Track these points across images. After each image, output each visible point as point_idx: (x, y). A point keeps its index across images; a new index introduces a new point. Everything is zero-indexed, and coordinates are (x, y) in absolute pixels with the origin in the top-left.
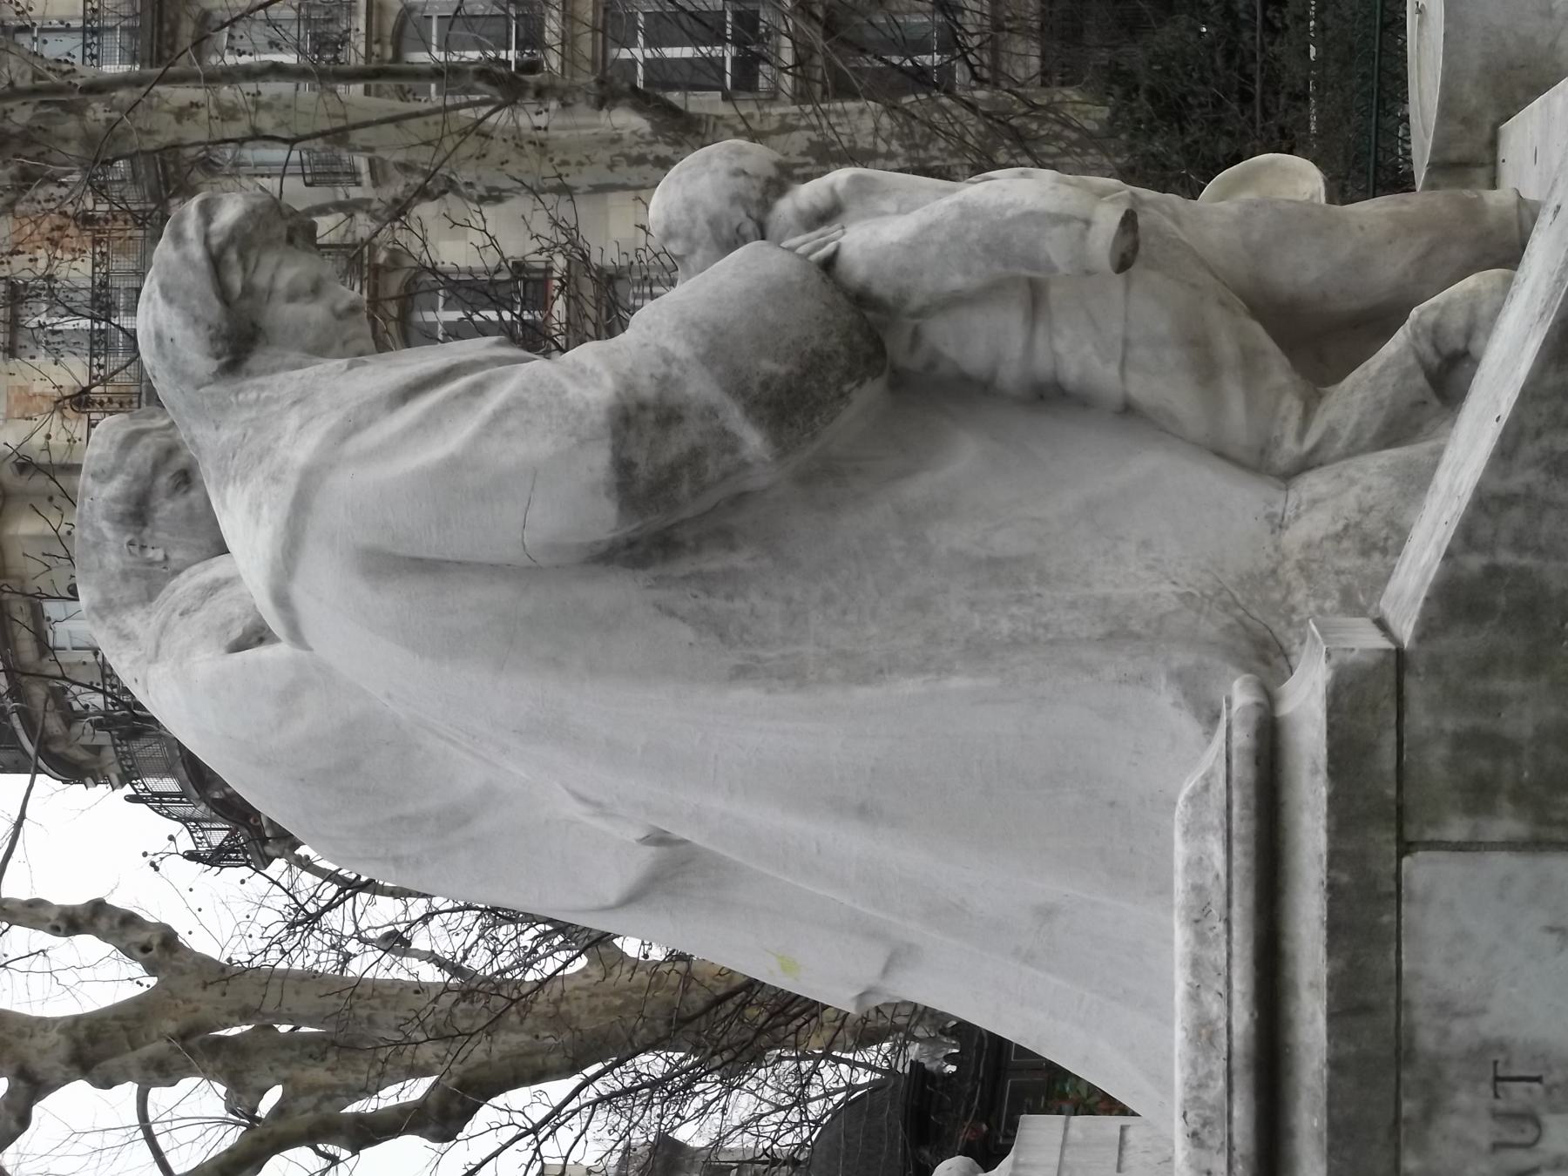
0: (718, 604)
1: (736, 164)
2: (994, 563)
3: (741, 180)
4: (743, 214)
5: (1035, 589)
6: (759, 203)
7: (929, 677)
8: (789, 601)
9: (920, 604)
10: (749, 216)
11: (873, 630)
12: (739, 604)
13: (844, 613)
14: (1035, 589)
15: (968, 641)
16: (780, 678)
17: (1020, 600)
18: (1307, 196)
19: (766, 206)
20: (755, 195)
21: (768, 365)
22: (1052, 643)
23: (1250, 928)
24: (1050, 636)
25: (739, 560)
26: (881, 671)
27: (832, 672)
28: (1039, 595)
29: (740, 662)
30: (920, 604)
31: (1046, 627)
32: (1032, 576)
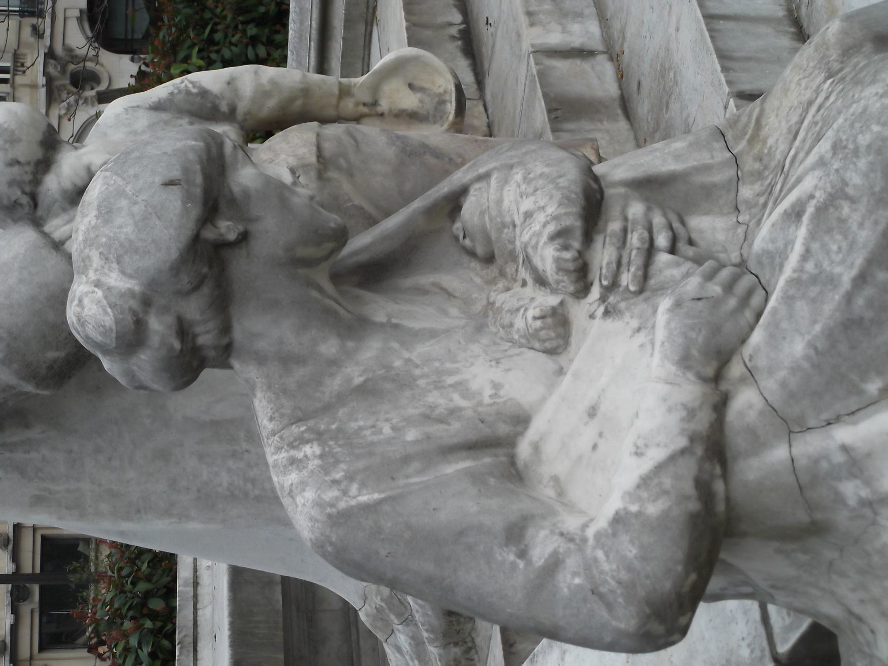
0: (19, 456)
1: (11, 155)
2: (215, 424)
3: (16, 169)
4: (19, 193)
5: (245, 446)
6: (30, 182)
7: (172, 520)
8: (70, 452)
9: (163, 455)
10: (24, 192)
11: (131, 474)
12: (34, 455)
13: (110, 459)
14: (245, 446)
15: (199, 491)
16: (67, 508)
17: (234, 455)
18: (441, 90)
19: (37, 181)
20: (28, 177)
21: (52, 355)
22: (258, 499)
23: (318, 5)
24: (257, 492)
25: (34, 433)
26: (138, 511)
27: (104, 507)
28: (247, 451)
29: (37, 493)
30: (163, 455)
31: (253, 481)
32: (242, 434)
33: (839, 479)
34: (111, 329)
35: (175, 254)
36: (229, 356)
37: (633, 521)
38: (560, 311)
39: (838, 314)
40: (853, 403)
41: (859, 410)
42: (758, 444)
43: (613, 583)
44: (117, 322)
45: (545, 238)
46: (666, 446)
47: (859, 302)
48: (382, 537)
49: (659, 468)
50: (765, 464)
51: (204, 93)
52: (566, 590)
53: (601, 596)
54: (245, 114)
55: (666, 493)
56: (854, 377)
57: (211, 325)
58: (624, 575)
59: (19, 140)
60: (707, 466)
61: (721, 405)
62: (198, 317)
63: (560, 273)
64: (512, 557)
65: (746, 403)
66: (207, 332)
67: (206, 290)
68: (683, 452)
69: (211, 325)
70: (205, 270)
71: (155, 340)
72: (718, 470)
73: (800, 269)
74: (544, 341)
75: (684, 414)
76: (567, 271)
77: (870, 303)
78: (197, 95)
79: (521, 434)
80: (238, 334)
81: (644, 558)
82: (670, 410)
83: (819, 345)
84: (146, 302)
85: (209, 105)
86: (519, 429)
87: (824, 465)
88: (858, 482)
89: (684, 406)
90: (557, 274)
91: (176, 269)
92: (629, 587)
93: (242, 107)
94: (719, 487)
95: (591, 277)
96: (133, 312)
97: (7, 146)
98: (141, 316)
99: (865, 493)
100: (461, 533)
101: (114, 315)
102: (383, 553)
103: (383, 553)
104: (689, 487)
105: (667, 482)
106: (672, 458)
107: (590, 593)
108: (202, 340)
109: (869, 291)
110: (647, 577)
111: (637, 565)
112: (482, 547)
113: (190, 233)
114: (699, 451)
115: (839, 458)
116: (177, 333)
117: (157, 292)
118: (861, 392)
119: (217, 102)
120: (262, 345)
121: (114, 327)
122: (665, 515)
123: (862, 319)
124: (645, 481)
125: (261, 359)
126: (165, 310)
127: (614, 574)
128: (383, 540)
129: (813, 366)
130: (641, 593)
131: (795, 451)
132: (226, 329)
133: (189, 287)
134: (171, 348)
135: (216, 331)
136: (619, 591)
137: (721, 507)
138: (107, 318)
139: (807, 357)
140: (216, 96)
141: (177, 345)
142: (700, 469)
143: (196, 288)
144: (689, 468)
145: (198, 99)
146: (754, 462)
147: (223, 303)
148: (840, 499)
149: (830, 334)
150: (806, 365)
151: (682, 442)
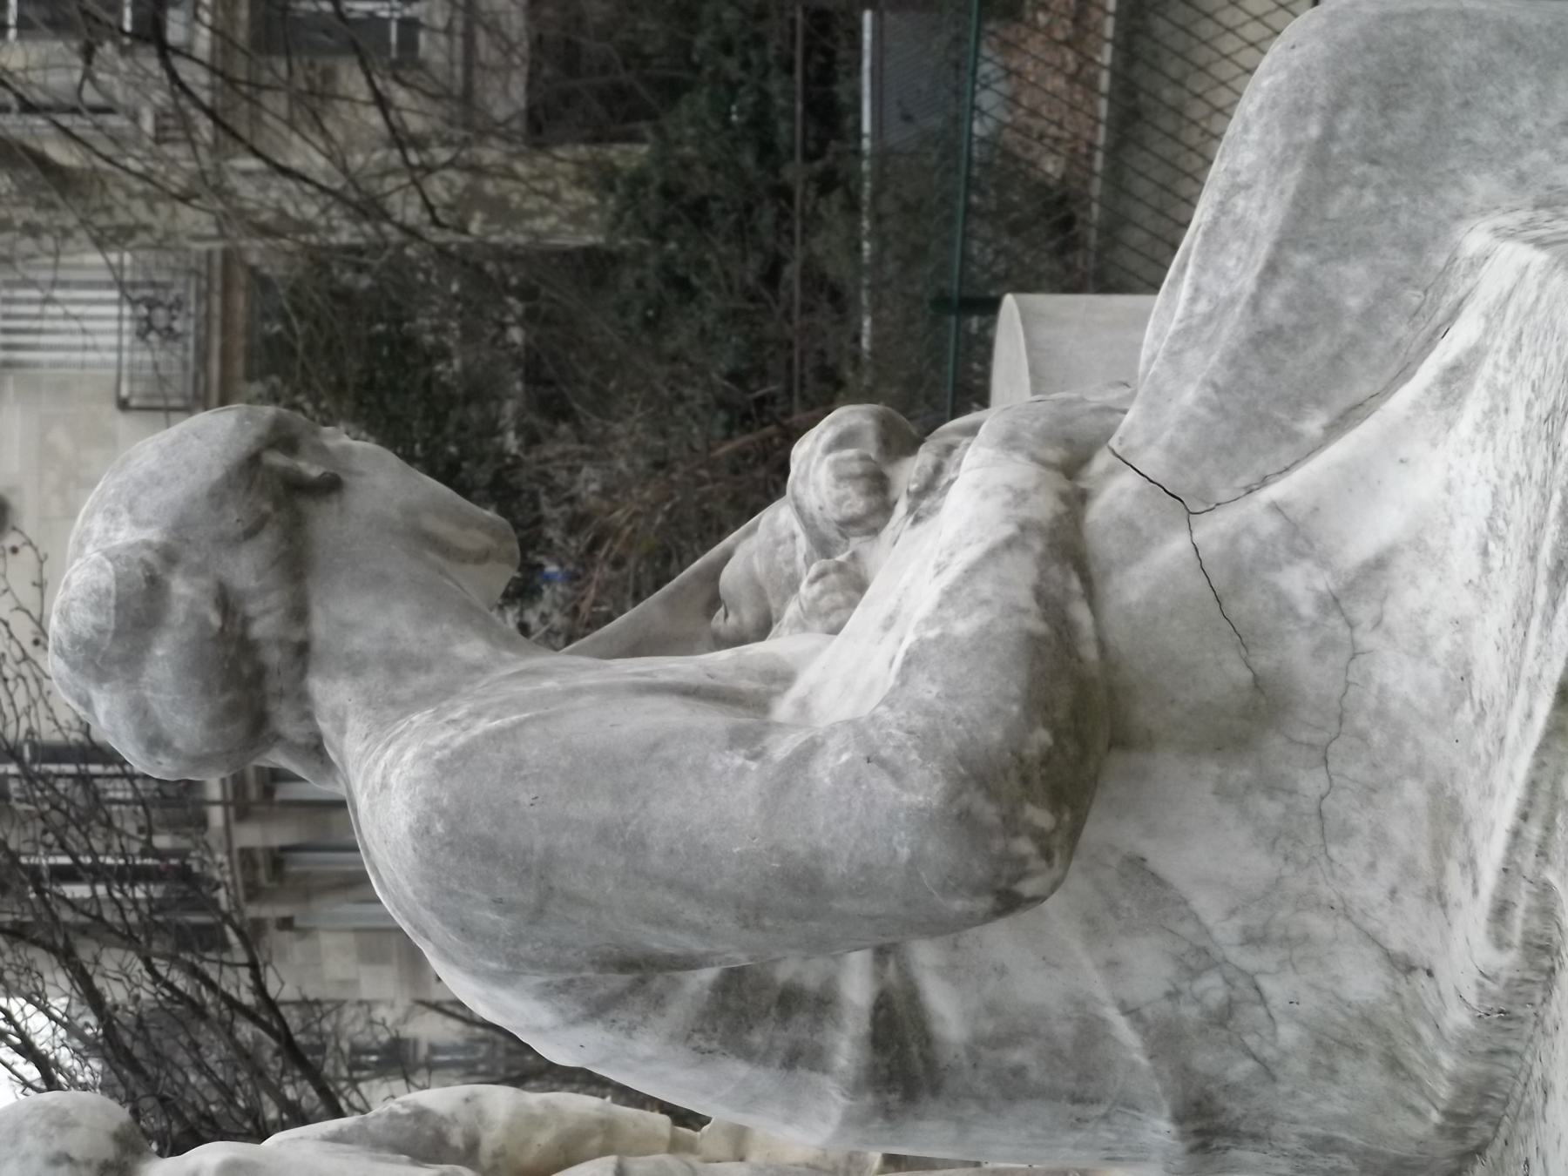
33: (1276, 566)
34: (108, 592)
35: (217, 474)
36: (303, 674)
37: (933, 651)
38: (851, 567)
39: (1242, 329)
40: (1285, 453)
41: (1297, 462)
42: (1139, 540)
43: (899, 734)
44: (118, 580)
45: (819, 452)
46: (981, 540)
47: (1273, 304)
48: (524, 773)
49: (971, 572)
50: (1150, 573)
51: (420, 1114)
52: (827, 780)
53: (883, 763)
54: (496, 1155)
55: (985, 602)
56: (1282, 415)
57: (273, 599)
58: (919, 722)
59: (74, 1125)
60: (1055, 571)
61: (1077, 500)
62: (253, 584)
63: (842, 485)
64: (739, 761)
65: (1115, 495)
66: (267, 612)
67: (267, 538)
68: (1009, 544)
69: (273, 599)
70: (267, 507)
71: (178, 613)
72: (1075, 584)
73: (1189, 314)
74: (827, 614)
75: (1009, 496)
76: (852, 478)
77: (1289, 304)
78: (408, 1116)
79: (779, 694)
80: (320, 627)
81: (951, 697)
82: (985, 496)
83: (1219, 380)
84: (169, 556)
85: (429, 1133)
86: (775, 687)
87: (1248, 544)
88: (1308, 565)
89: (1009, 488)
90: (837, 487)
91: (218, 496)
92: (927, 741)
93: (490, 1140)
94: (1081, 613)
95: (893, 494)
96: (147, 566)
97: (53, 1131)
98: (159, 572)
99: (1323, 582)
100: (655, 746)
101: (115, 567)
102: (525, 799)
103: (525, 799)
104: (1024, 597)
105: (986, 588)
106: (992, 554)
107: (864, 765)
108: (258, 630)
109: (1285, 286)
110: (959, 720)
111: (941, 706)
112: (689, 760)
113: (244, 449)
114: (1038, 545)
115: (1269, 526)
116: (216, 601)
117: (188, 541)
118: (1294, 437)
119: (444, 1128)
120: (357, 642)
121: (113, 587)
122: (985, 632)
123: (1279, 328)
124: (950, 595)
125: (355, 666)
126: (200, 570)
127: (902, 721)
128: (525, 778)
129: (1213, 410)
130: (950, 745)
131: (1197, 536)
132: (299, 613)
133: (240, 528)
134: (204, 624)
135: (282, 611)
136: (909, 744)
137: (1090, 652)
138: (104, 575)
139: (1202, 401)
140: (442, 1118)
141: (215, 620)
142: (1043, 575)
143: (251, 533)
144: (1022, 572)
145: (409, 1124)
146: (1136, 571)
147: (295, 565)
148: (1286, 608)
149: (1232, 360)
150: (1202, 412)
151: (1009, 530)
